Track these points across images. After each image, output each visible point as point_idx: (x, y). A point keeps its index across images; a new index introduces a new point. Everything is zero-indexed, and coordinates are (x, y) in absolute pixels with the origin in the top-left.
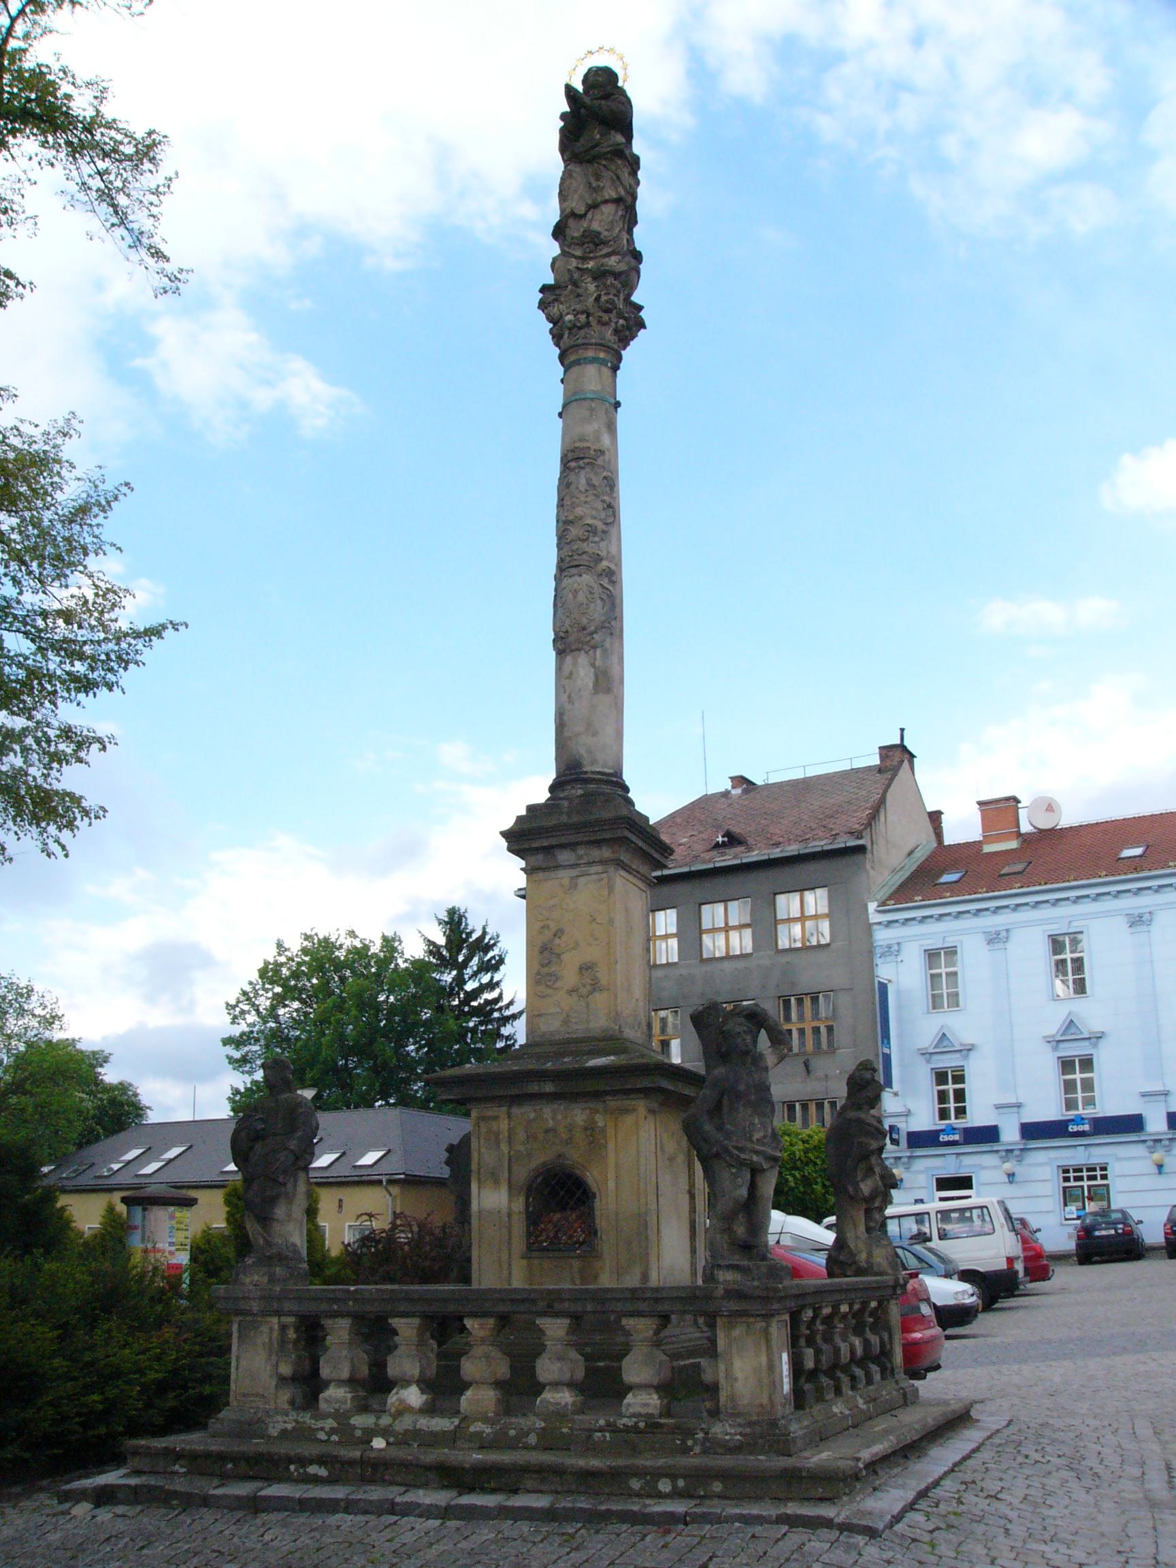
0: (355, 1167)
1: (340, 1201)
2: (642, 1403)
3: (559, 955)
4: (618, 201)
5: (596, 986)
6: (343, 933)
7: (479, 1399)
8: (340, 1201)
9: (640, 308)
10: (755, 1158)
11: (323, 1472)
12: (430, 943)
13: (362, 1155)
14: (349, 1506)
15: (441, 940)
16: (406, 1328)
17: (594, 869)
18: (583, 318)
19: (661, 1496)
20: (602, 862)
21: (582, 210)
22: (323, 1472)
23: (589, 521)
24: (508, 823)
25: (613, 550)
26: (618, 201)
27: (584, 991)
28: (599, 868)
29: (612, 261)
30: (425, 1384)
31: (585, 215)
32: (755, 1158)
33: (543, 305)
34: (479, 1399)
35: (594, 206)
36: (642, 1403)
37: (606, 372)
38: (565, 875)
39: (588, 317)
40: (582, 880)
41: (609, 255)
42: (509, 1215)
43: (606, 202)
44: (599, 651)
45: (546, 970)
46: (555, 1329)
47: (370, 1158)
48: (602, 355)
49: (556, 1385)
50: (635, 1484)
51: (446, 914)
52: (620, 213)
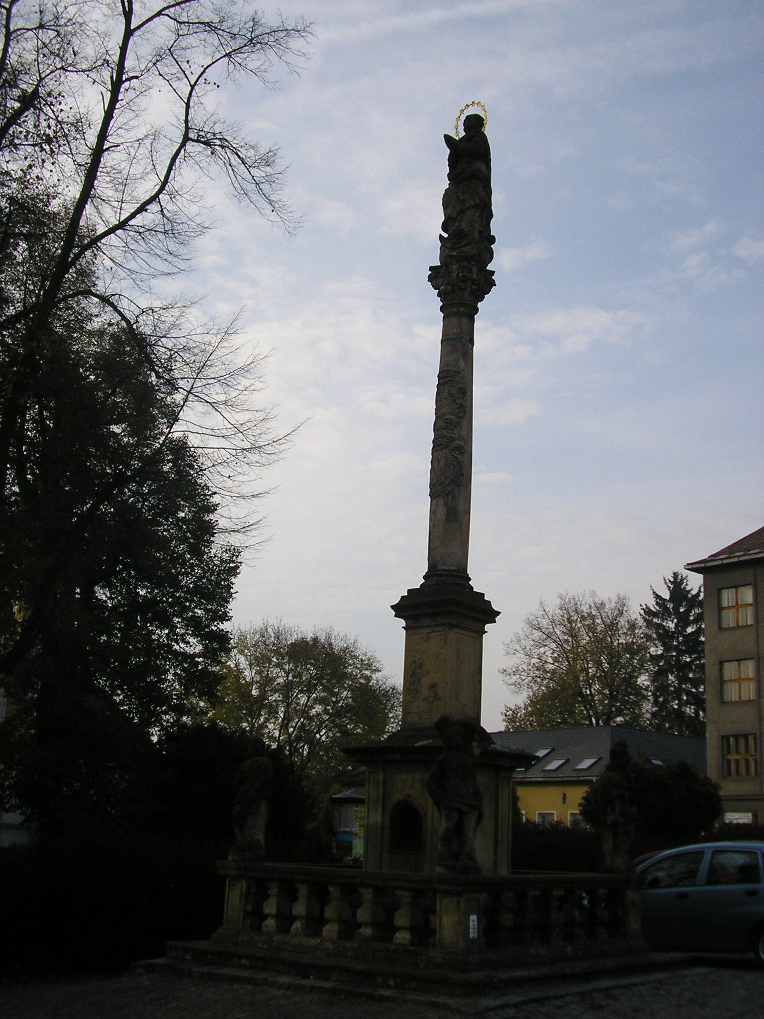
0: (544, 771)
1: (565, 795)
2: (402, 937)
3: (419, 679)
4: (476, 207)
5: (436, 697)
6: (588, 594)
7: (331, 930)
8: (565, 795)
9: (493, 273)
10: (459, 805)
11: (247, 963)
12: (657, 596)
13: (580, 762)
14: (249, 981)
15: (666, 595)
16: (303, 891)
17: (437, 629)
18: (449, 287)
19: (389, 987)
20: (442, 625)
21: (455, 215)
22: (247, 963)
23: (448, 417)
24: (396, 601)
25: (464, 433)
26: (476, 207)
27: (430, 700)
28: (440, 628)
29: (467, 249)
30: (373, 924)
31: (456, 218)
32: (459, 805)
33: (430, 279)
34: (331, 930)
35: (462, 212)
36: (402, 937)
37: (464, 320)
38: (424, 632)
39: (453, 286)
40: (432, 635)
41: (465, 245)
42: (382, 827)
43: (469, 208)
44: (450, 497)
45: (413, 687)
46: (367, 894)
47: (586, 764)
48: (462, 309)
49: (366, 924)
50: (379, 980)
51: (558, 602)
52: (477, 214)
